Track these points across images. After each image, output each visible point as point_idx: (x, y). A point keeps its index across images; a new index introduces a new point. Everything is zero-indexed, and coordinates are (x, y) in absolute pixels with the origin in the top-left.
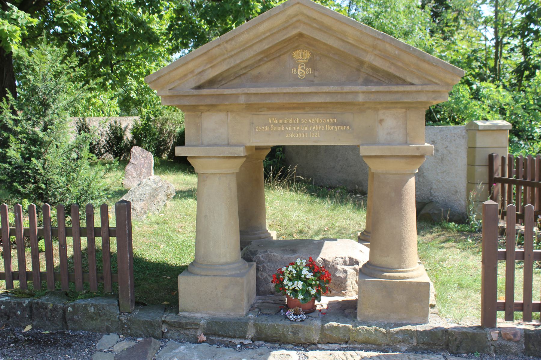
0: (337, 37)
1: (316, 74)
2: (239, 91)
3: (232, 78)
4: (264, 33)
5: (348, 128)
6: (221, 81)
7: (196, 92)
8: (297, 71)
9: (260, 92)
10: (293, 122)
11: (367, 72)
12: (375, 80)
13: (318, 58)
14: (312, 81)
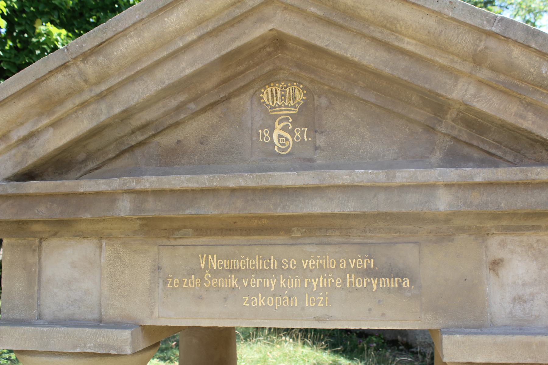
0: (373, 39)
1: (320, 141)
2: (116, 184)
3: (111, 156)
4: (181, 33)
5: (406, 283)
6: (84, 161)
7: (12, 188)
8: (271, 135)
9: (167, 187)
10: (260, 265)
11: (455, 133)
12: (476, 154)
13: (324, 101)
14: (311, 160)
